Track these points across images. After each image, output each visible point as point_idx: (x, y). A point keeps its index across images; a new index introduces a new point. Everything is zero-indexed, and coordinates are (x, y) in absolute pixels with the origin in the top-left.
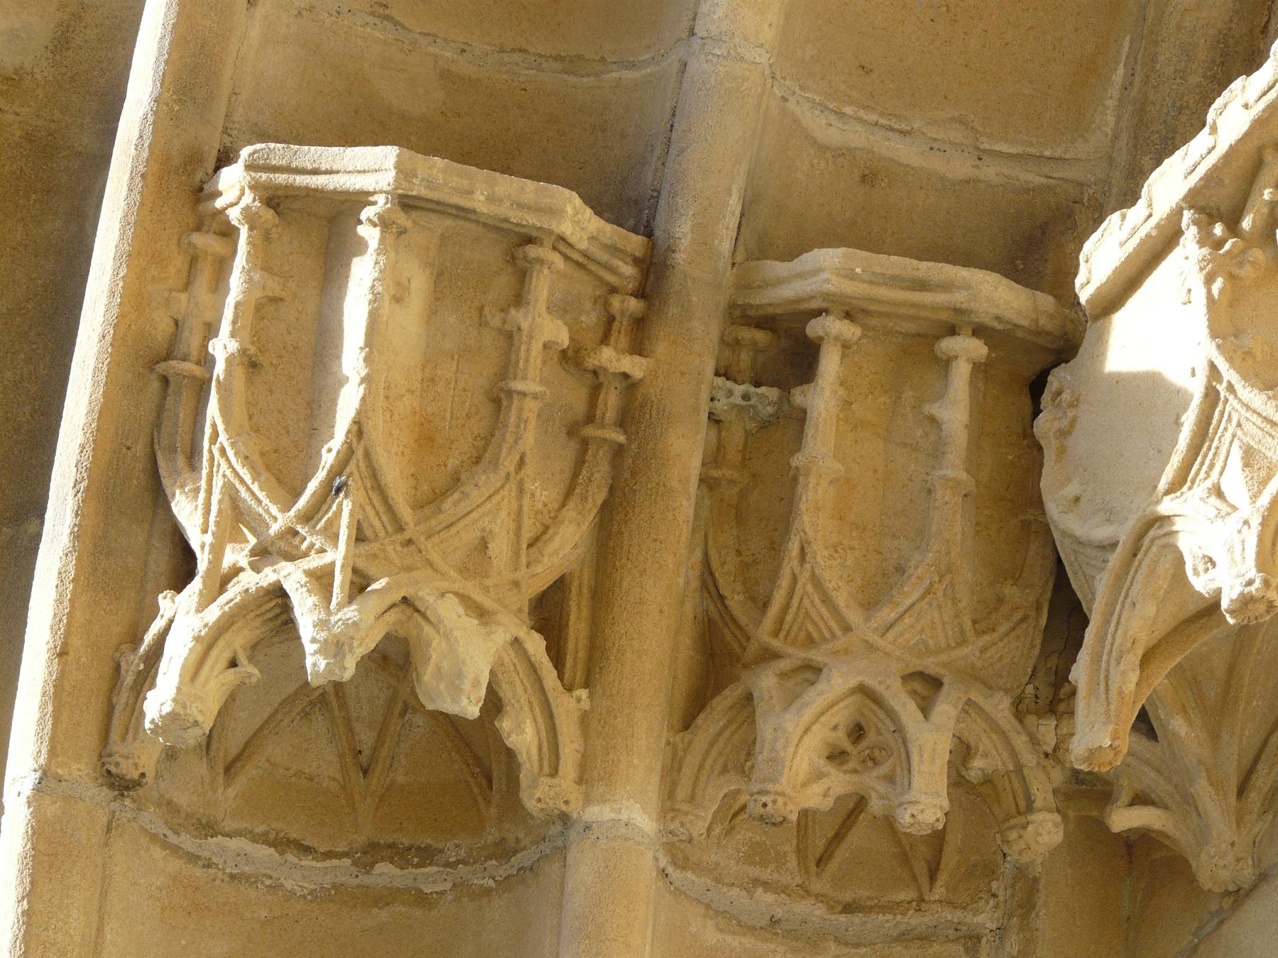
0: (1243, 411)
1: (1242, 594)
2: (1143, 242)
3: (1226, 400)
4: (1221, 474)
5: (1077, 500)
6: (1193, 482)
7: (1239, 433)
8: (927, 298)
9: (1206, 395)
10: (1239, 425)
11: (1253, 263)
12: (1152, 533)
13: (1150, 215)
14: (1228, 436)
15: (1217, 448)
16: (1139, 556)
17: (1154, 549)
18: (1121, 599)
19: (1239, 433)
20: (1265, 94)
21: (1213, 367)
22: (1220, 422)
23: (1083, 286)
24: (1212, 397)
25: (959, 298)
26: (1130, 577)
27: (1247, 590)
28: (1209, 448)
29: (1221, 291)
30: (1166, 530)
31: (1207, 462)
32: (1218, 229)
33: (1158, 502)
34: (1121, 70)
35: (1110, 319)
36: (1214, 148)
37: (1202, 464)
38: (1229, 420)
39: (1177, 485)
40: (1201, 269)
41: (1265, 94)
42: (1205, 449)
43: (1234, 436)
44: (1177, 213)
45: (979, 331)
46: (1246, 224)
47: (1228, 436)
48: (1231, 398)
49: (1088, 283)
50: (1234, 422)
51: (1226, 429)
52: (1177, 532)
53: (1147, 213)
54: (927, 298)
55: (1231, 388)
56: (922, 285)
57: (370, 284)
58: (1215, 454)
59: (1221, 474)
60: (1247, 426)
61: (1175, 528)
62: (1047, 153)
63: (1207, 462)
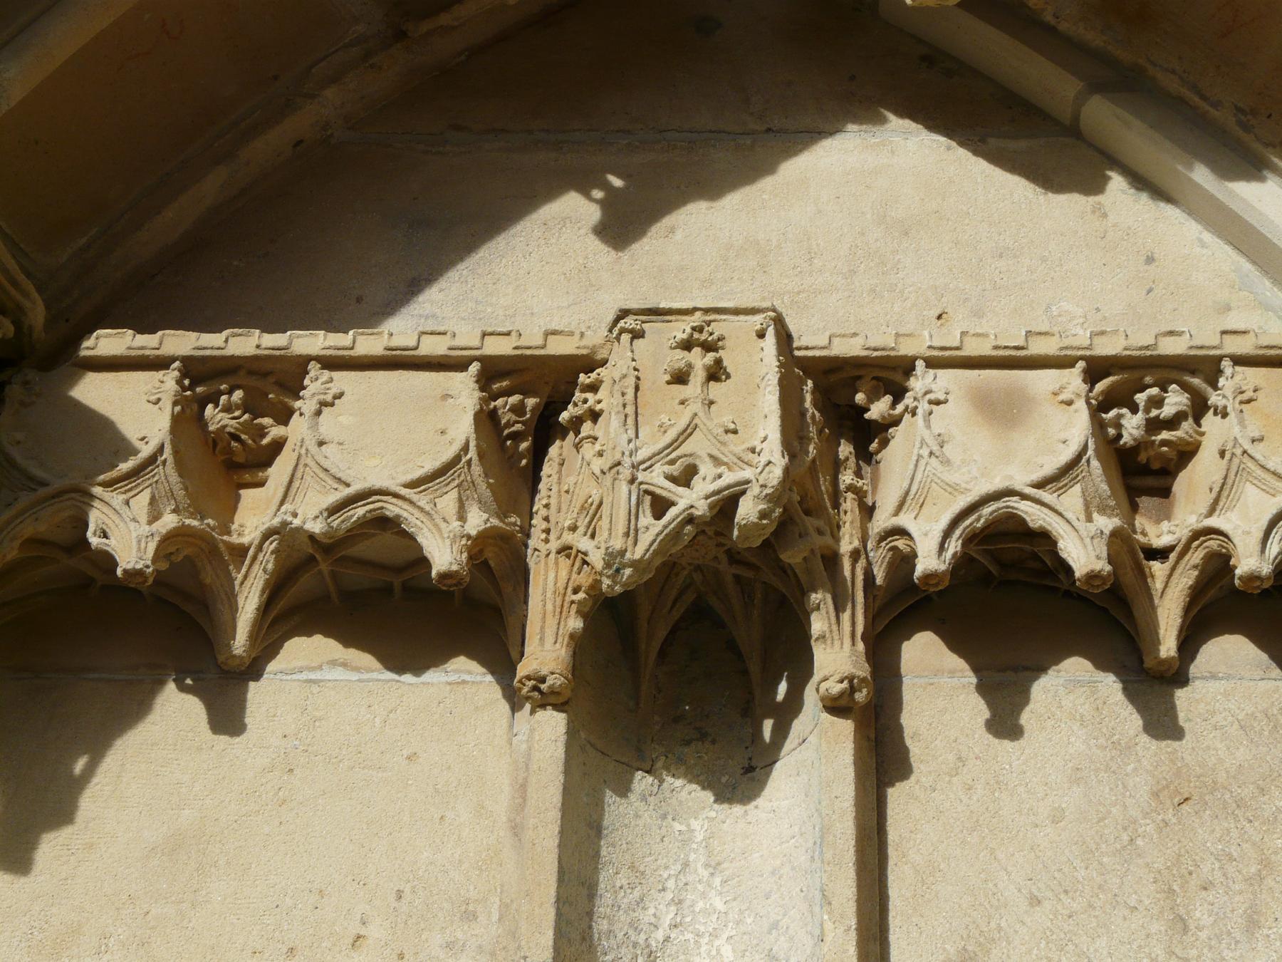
0: (163, 478)
1: (141, 569)
2: (143, 356)
3: (158, 466)
4: (133, 497)
5: (19, 442)
6: (115, 489)
7: (154, 485)
8: (13, 292)
9: (151, 457)
10: (157, 482)
11: (192, 410)
12: (73, 495)
13: (158, 349)
14: (149, 482)
15: (139, 484)
16: (56, 500)
17: (69, 503)
18: (31, 512)
19: (154, 485)
20: (273, 349)
21: (162, 446)
22: (149, 473)
23: (88, 348)
24: (152, 460)
25: (27, 304)
26: (43, 505)
27: (145, 569)
28: (135, 481)
29: (178, 412)
30: (86, 500)
31: (130, 486)
32: (187, 382)
33: (93, 485)
34: (84, 240)
35: (84, 374)
36: (222, 349)
37: (126, 485)
38: (153, 476)
39: (107, 484)
40: (175, 396)
41: (273, 349)
42: (132, 480)
43: (151, 485)
44: (173, 359)
45: (18, 324)
46: (199, 390)
47: (149, 482)
48: (161, 467)
49: (92, 349)
50: (155, 479)
51: (149, 479)
52: (93, 506)
53: (157, 347)
54: (13, 292)
55: (164, 462)
56: (15, 283)
57: (728, 381)
58: (136, 486)
59: (133, 497)
60: (160, 486)
61: (93, 504)
62: (22, 246)
63: (130, 486)
